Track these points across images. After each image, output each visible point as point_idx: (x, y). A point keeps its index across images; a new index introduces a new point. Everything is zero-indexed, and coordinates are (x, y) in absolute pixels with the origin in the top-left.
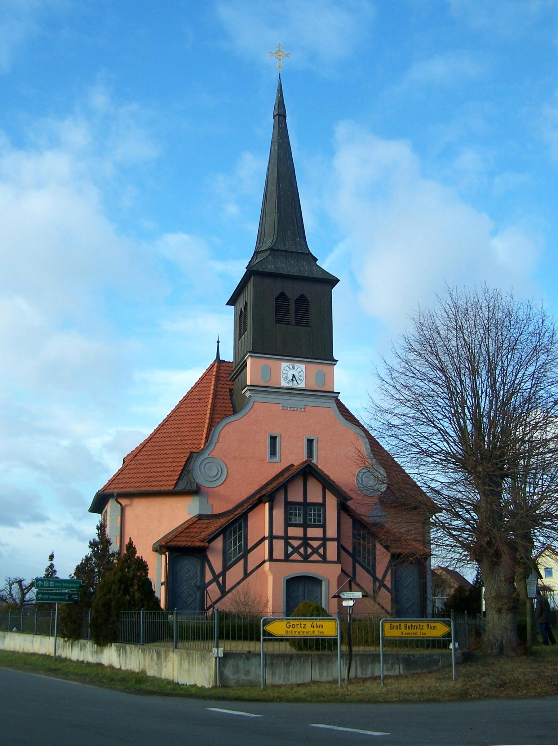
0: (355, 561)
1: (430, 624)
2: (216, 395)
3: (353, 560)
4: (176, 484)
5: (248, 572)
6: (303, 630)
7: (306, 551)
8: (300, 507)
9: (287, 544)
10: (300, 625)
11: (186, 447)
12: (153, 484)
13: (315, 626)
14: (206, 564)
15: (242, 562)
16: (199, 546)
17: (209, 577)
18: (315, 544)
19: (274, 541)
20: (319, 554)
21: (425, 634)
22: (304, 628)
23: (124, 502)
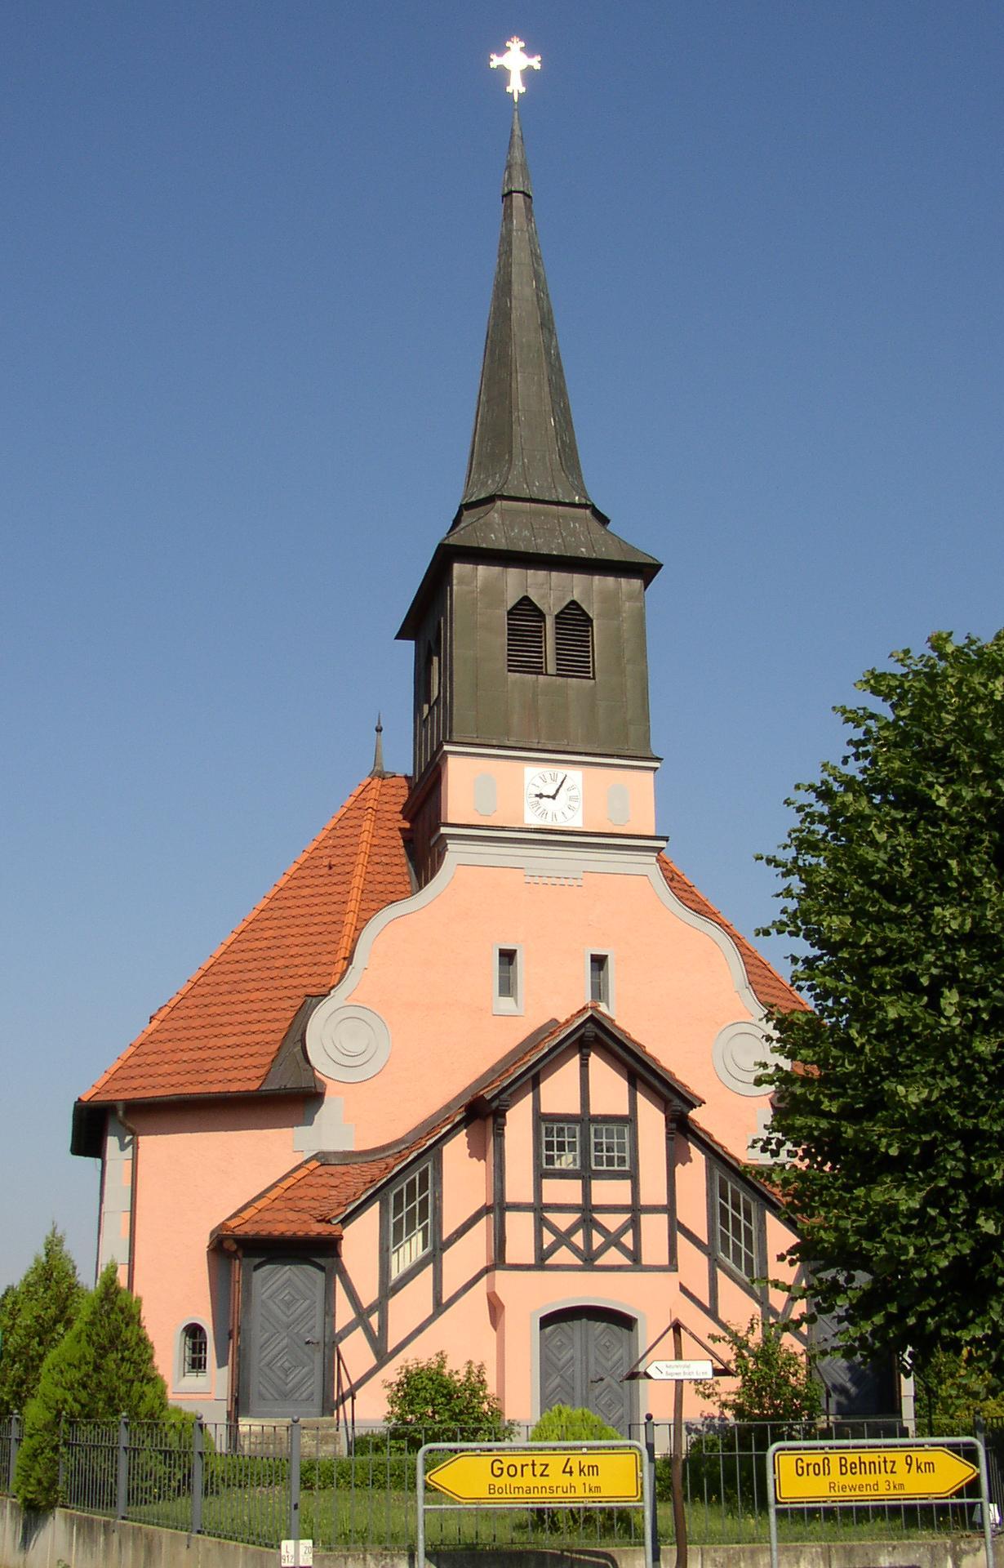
3: (709, 1259)
5: (444, 1301)
6: (540, 1482)
7: (588, 1239)
8: (610, 1127)
9: (541, 1223)
10: (531, 1467)
13: (576, 1470)
15: (430, 1269)
16: (319, 1234)
17: (344, 1313)
18: (613, 1222)
19: (509, 1215)
21: (901, 1485)
22: (542, 1475)
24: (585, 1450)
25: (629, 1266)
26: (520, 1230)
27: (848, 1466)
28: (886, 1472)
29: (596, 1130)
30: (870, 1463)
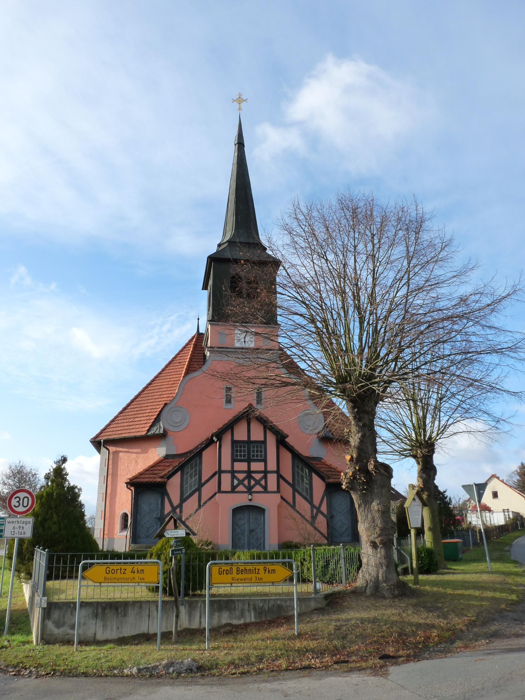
0: (295, 490)
1: (267, 567)
2: (192, 359)
4: (148, 431)
7: (249, 482)
9: (233, 477)
11: (163, 399)
12: (132, 431)
13: (136, 571)
14: (166, 497)
15: (197, 494)
16: (159, 482)
17: (168, 508)
18: (258, 476)
19: (222, 474)
20: (261, 486)
21: (262, 579)
22: (124, 573)
23: (112, 449)
24: (101, 564)
25: (199, 493)
26: (226, 479)
27: (240, 571)
28: (255, 573)
29: (236, 445)
30: (249, 570)
